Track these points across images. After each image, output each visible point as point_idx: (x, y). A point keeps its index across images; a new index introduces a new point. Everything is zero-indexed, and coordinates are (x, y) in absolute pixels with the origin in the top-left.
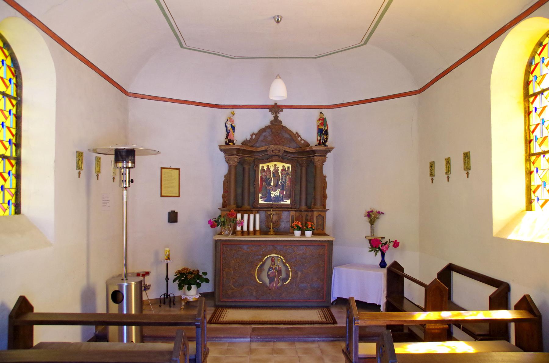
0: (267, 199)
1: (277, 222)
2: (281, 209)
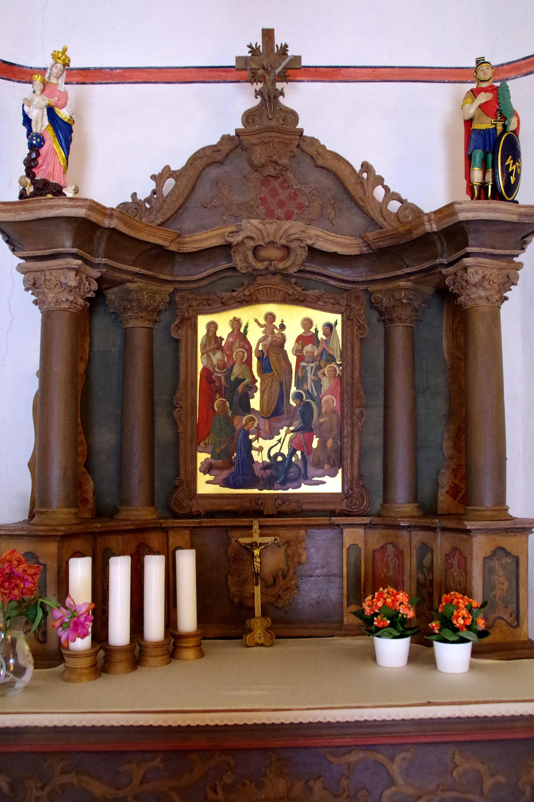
0: (234, 475)
1: (284, 577)
2: (299, 521)
